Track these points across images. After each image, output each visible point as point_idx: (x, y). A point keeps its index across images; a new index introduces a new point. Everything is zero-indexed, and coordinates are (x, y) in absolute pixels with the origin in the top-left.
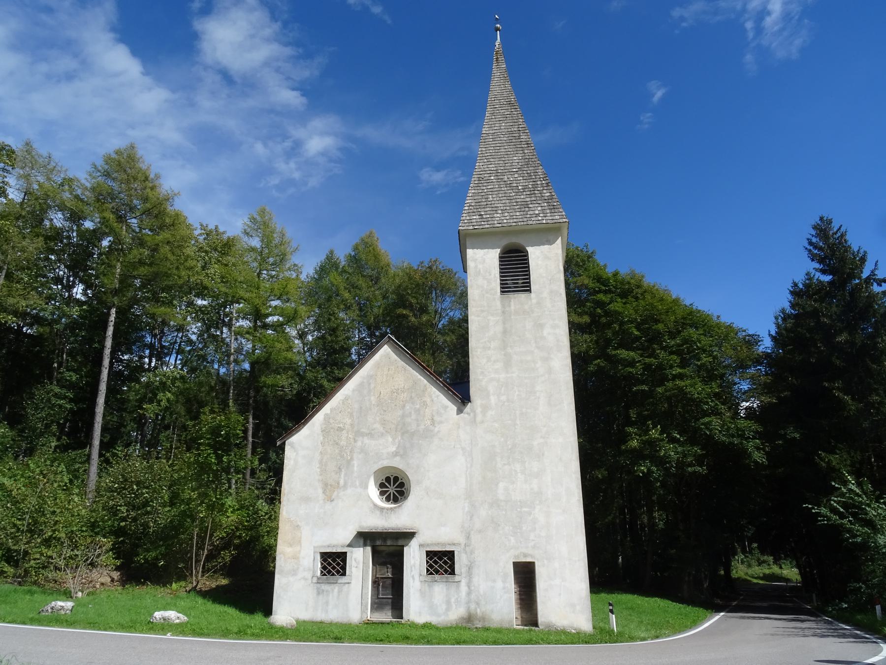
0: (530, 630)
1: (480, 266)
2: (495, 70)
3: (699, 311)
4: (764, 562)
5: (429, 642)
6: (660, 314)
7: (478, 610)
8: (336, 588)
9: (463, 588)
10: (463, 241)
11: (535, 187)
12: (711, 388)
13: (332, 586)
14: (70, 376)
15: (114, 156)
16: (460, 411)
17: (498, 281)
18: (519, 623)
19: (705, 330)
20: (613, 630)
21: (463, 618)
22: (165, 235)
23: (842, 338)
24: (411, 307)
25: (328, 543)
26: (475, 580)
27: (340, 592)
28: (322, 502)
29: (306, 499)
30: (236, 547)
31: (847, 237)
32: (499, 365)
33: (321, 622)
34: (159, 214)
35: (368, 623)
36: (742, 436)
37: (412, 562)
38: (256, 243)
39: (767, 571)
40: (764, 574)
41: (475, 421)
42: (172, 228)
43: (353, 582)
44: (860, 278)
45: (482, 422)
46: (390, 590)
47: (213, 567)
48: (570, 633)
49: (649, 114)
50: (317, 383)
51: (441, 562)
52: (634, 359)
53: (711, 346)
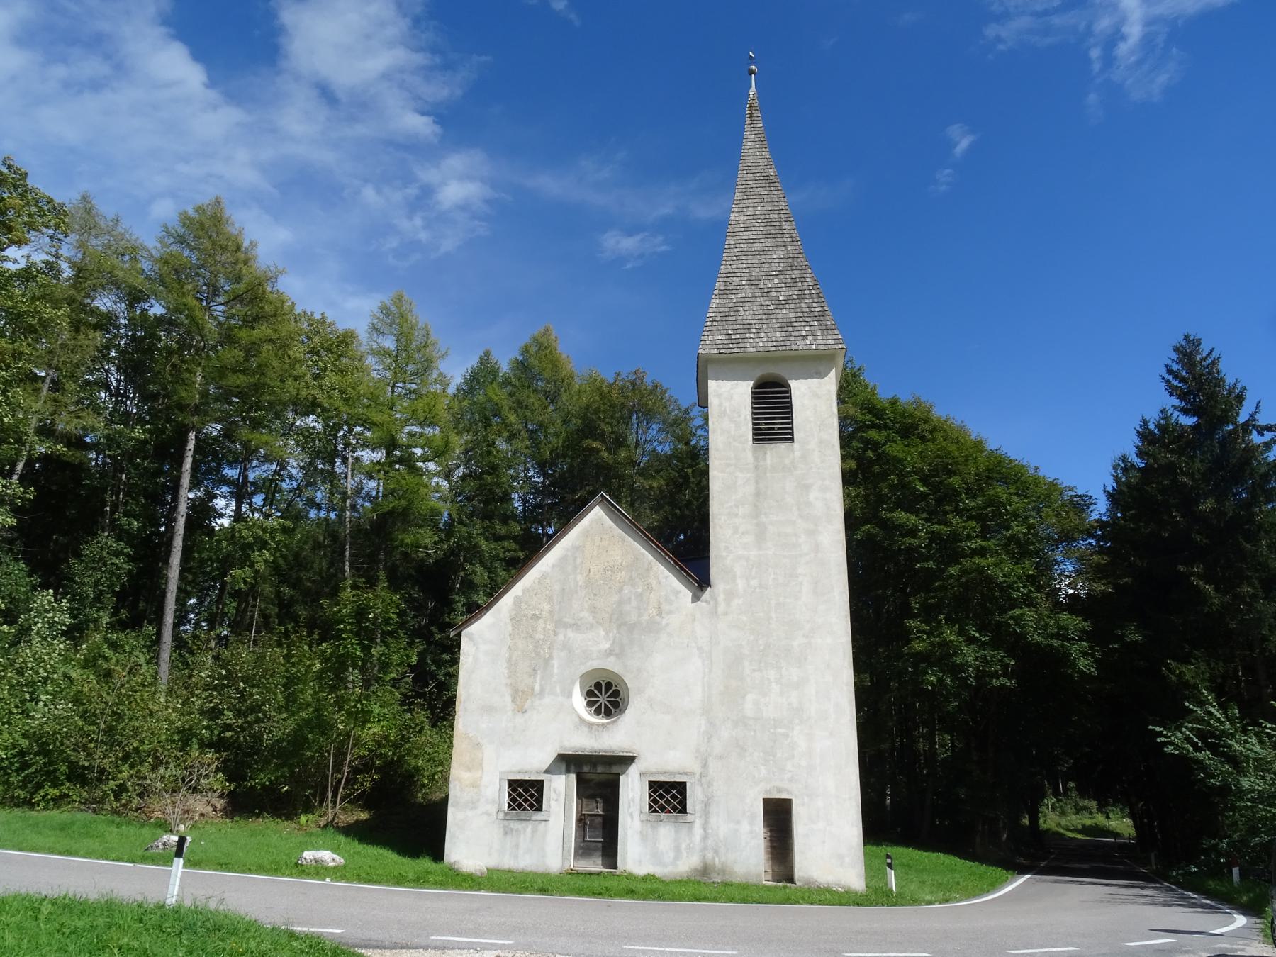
0: (785, 887)
1: (726, 404)
2: (748, 131)
4: (1084, 808)
5: (659, 898)
8: (529, 827)
9: (698, 830)
10: (703, 370)
11: (801, 297)
13: (524, 824)
16: (696, 598)
19: (1018, 488)
21: (696, 870)
23: (1207, 505)
24: (601, 437)
25: (518, 768)
26: (713, 820)
27: (534, 832)
28: (510, 713)
29: (489, 709)
30: (378, 770)
31: (1220, 366)
34: (255, 301)
35: (572, 873)
36: (1065, 638)
37: (631, 796)
38: (389, 343)
39: (1088, 822)
40: (1084, 826)
42: (273, 320)
44: (1235, 423)
45: (726, 614)
46: (600, 832)
48: (836, 892)
49: (947, 171)
51: (669, 797)
53: (1026, 510)
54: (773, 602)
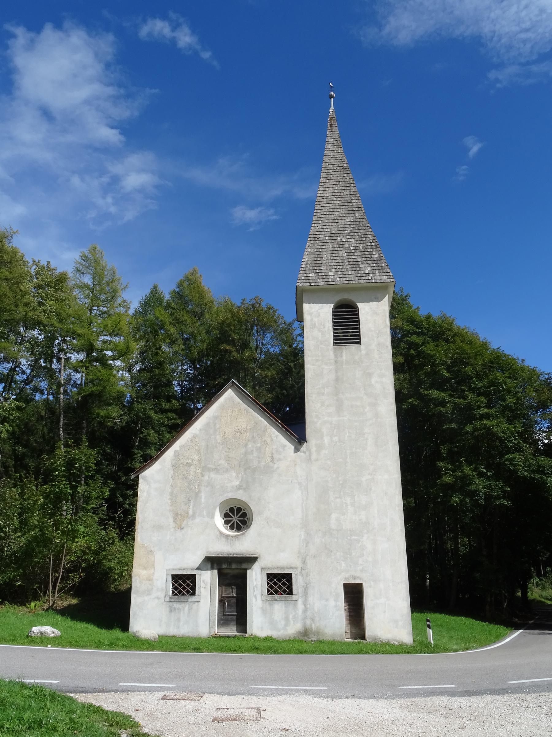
0: (359, 643)
1: (315, 320)
2: (329, 136)
3: (505, 355)
5: (275, 652)
6: (469, 358)
7: (313, 625)
8: (186, 607)
10: (300, 297)
11: (365, 248)
12: (515, 427)
13: (183, 604)
18: (349, 636)
19: (510, 373)
20: (430, 643)
21: (299, 633)
25: (179, 567)
26: (310, 599)
27: (190, 609)
28: (172, 530)
29: (159, 527)
30: (84, 570)
32: (332, 410)
33: (174, 636)
37: (255, 583)
38: (88, 280)
41: (310, 459)
43: (202, 601)
45: (317, 460)
46: (235, 608)
49: (464, 167)
50: (145, 414)
51: (281, 584)
52: (444, 399)
54: (348, 452)
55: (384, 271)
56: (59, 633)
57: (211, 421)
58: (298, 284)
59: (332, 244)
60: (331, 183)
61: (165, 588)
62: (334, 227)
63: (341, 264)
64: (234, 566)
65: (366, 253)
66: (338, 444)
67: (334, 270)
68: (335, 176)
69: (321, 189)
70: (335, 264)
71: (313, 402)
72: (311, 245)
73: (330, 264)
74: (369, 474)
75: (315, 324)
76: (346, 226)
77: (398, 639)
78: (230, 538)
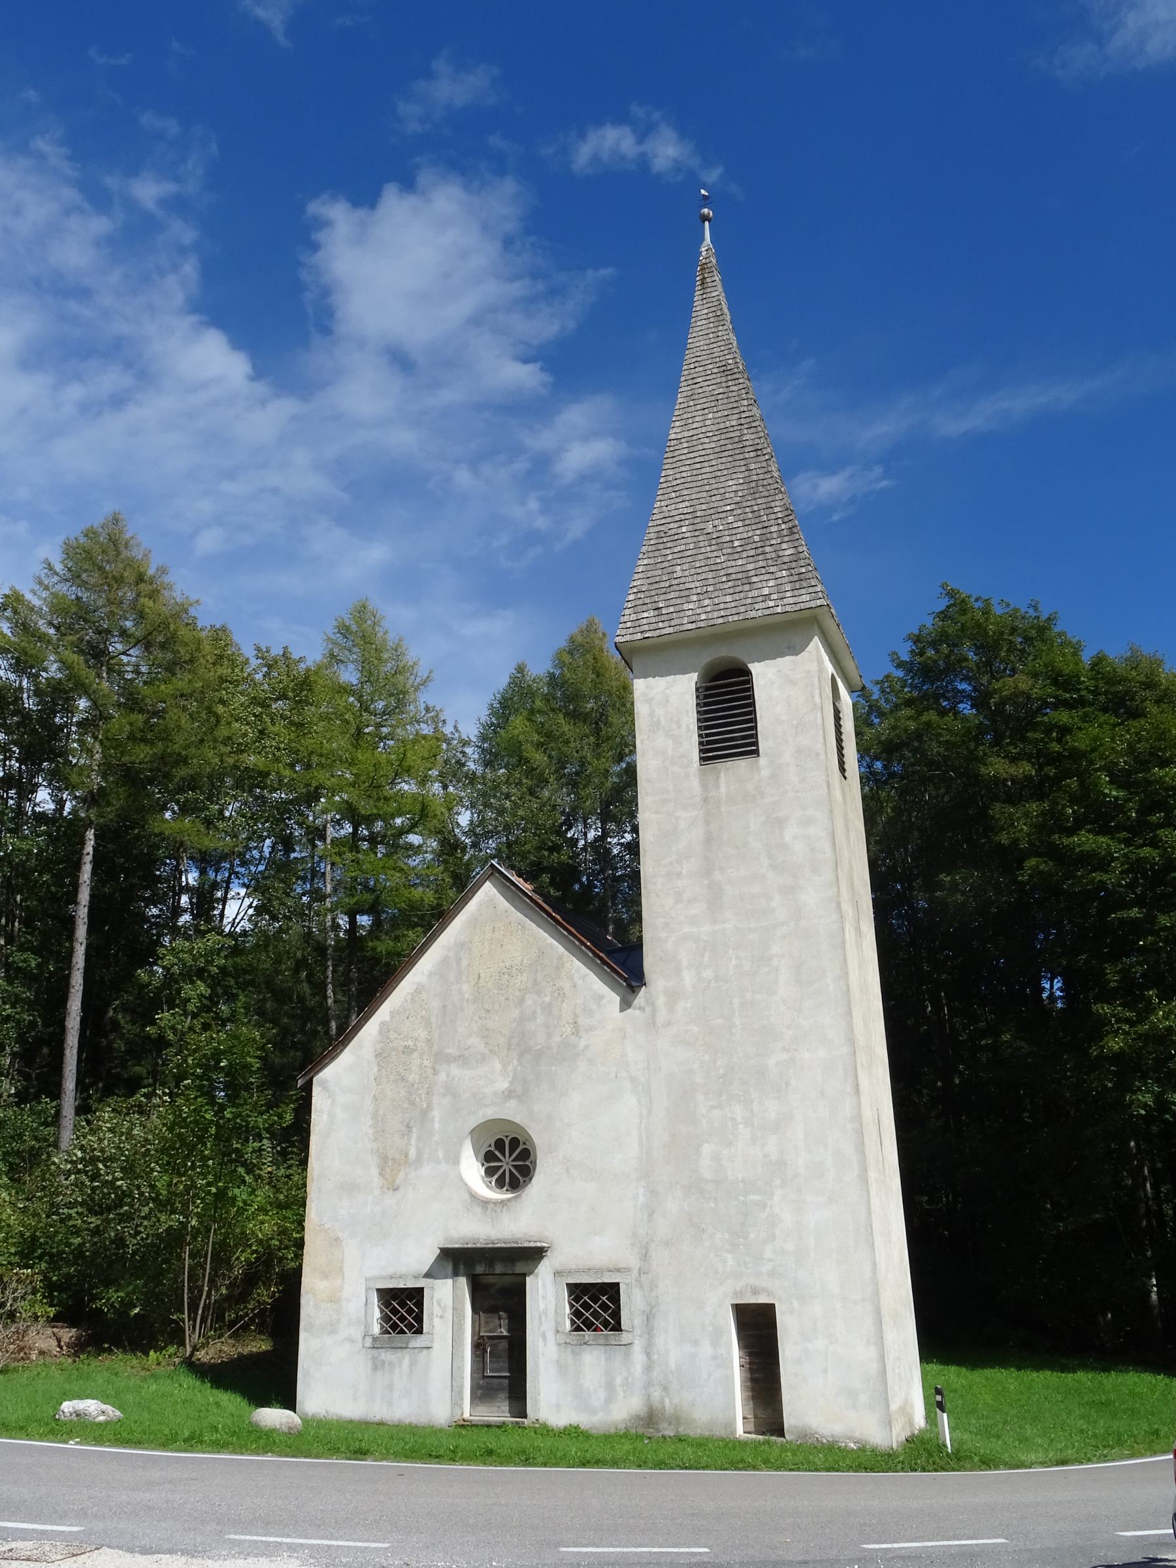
1: (660, 712)
5: (527, 1462)
7: (667, 1401)
8: (406, 1357)
13: (399, 1353)
14: (25, 961)
15: (82, 540)
17: (695, 739)
18: (751, 1427)
20: (945, 1446)
21: (638, 1417)
22: (182, 681)
25: (390, 1271)
26: (660, 1341)
27: (412, 1364)
28: (377, 1192)
29: (350, 1188)
33: (381, 1424)
38: (349, 675)
41: (654, 1023)
43: (436, 1346)
45: (668, 1024)
46: (503, 1364)
47: (238, 1319)
51: (597, 1306)
54: (736, 1001)
55: (804, 584)
56: (118, 1413)
57: (451, 954)
58: (618, 639)
59: (695, 539)
60: (698, 407)
61: (363, 1318)
62: (703, 501)
63: (711, 581)
64: (499, 1268)
65: (768, 549)
66: (713, 984)
67: (695, 598)
68: (708, 389)
69: (677, 424)
70: (698, 584)
71: (658, 896)
72: (651, 548)
73: (687, 586)
74: (784, 1049)
75: (659, 721)
76: (727, 495)
77: (857, 1435)
78: (490, 1206)
